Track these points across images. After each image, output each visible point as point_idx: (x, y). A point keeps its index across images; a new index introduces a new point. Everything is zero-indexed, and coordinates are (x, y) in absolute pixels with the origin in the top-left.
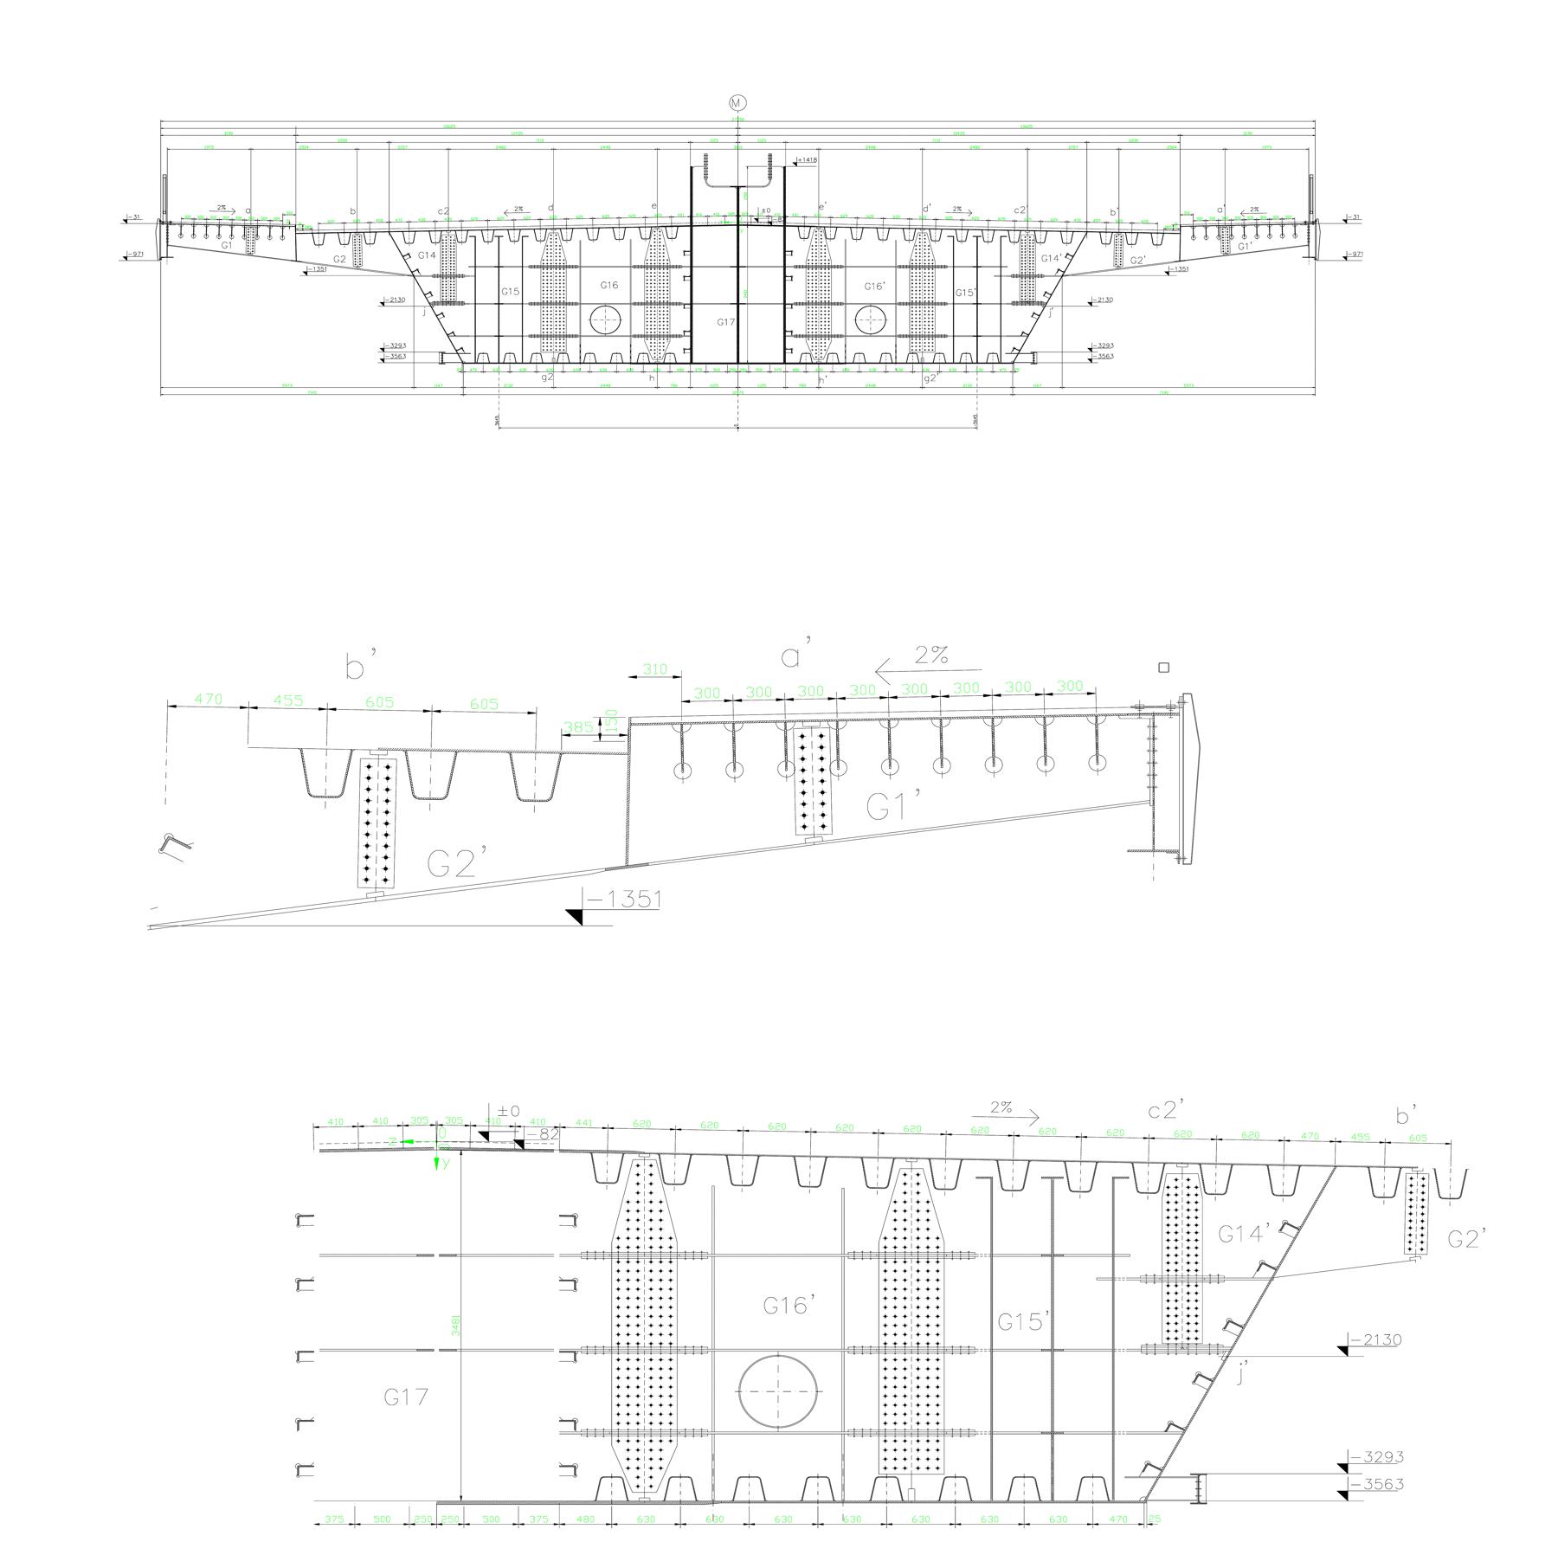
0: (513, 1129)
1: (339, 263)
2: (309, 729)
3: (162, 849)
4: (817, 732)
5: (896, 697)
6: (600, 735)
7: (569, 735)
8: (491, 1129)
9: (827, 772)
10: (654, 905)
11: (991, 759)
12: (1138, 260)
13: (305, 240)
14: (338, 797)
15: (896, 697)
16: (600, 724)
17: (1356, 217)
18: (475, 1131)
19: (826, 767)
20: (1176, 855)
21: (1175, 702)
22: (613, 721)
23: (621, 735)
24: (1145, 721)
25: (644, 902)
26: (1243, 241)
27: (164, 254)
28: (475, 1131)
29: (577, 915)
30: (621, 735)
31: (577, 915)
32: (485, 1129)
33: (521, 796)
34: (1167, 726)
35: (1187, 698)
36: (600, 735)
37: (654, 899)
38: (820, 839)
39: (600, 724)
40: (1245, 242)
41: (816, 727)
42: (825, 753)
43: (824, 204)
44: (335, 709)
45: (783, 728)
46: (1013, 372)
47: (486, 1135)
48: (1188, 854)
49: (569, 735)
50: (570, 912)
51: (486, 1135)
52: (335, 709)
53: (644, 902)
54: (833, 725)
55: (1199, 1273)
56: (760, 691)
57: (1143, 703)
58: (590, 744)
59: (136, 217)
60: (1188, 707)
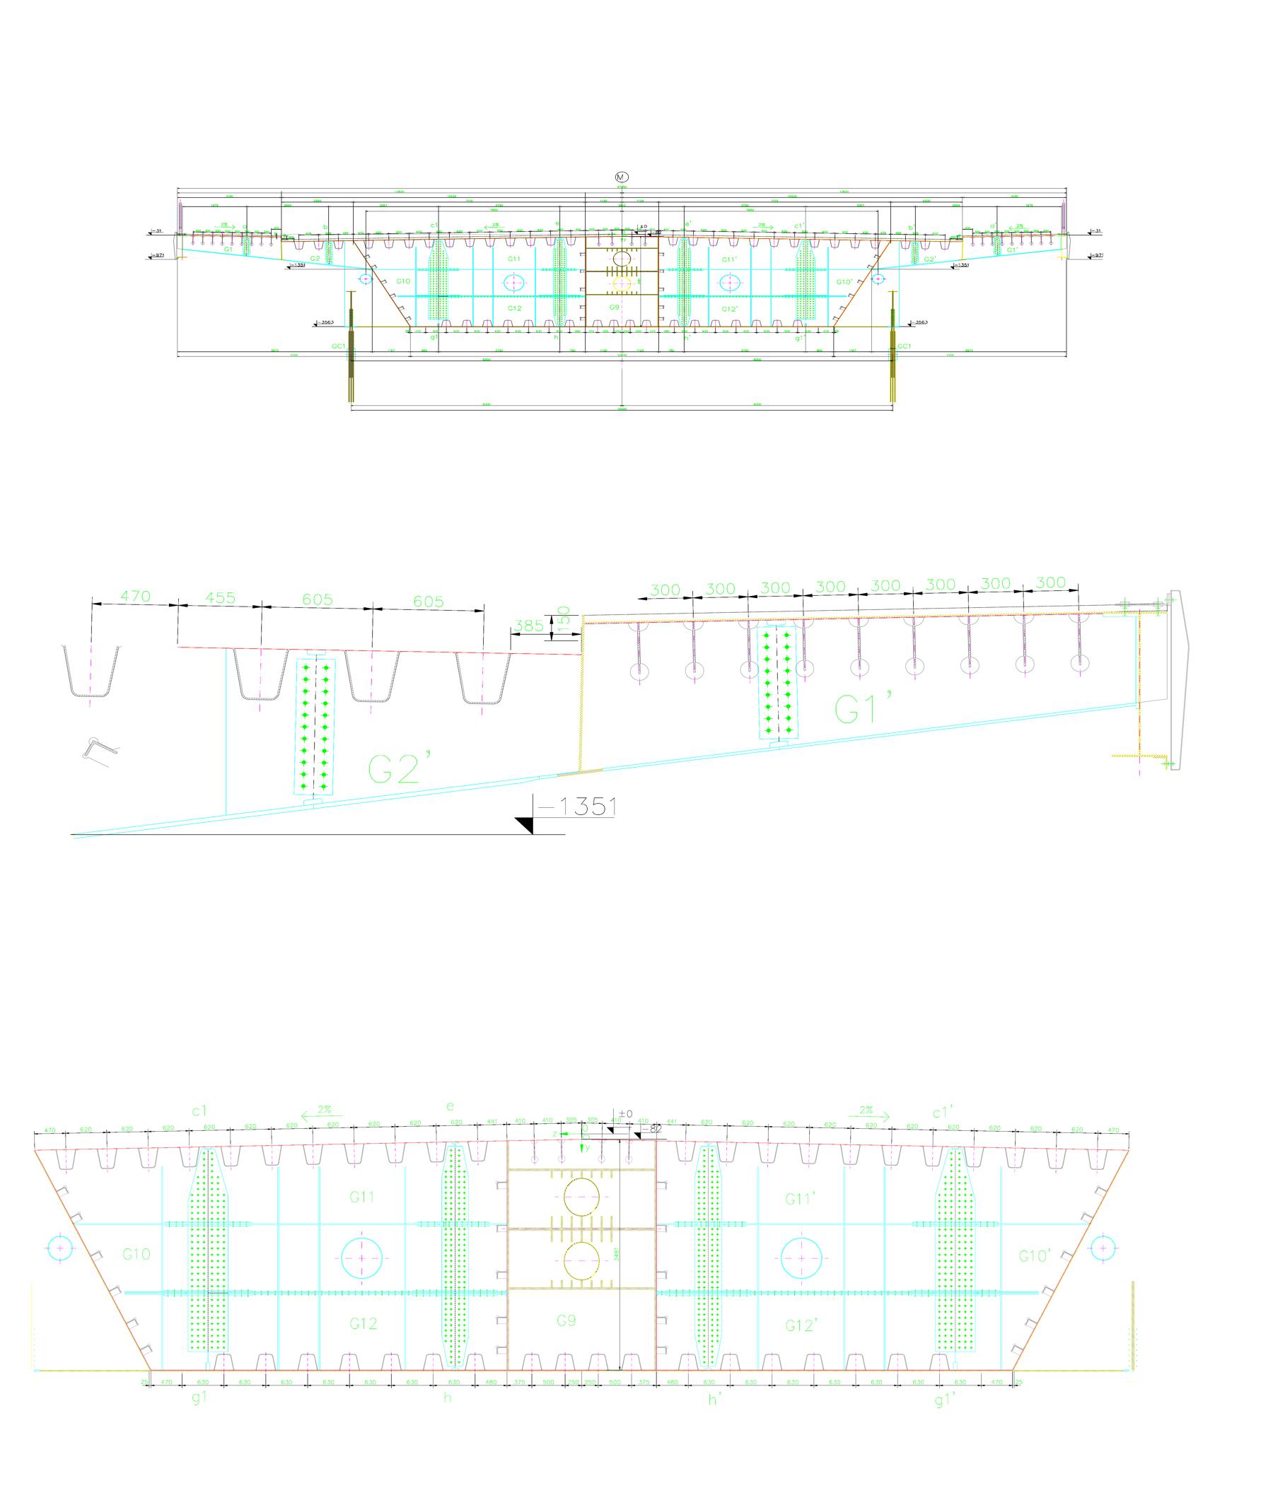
0: (628, 1126)
1: (314, 259)
2: (243, 627)
3: (86, 754)
4: (781, 631)
5: (976, 592)
6: (552, 634)
7: (518, 634)
8: (615, 1125)
9: (793, 673)
10: (609, 813)
11: (857, 662)
12: (930, 259)
13: (288, 246)
14: (354, 698)
15: (976, 592)
16: (552, 622)
17: (1098, 231)
18: (605, 1127)
19: (792, 668)
20: (1163, 760)
21: (1163, 599)
22: (565, 619)
23: (574, 634)
24: (1130, 621)
25: (599, 809)
26: (1011, 246)
27: (179, 255)
28: (605, 1127)
29: (527, 823)
30: (574, 634)
31: (527, 823)
32: (611, 1126)
33: (385, 698)
34: (1154, 625)
35: (1176, 596)
36: (552, 634)
37: (609, 806)
38: (785, 744)
39: (552, 622)
40: (1013, 247)
41: (782, 626)
42: (790, 653)
43: (689, 222)
44: (365, 609)
45: (747, 628)
46: (834, 332)
47: (611, 1129)
48: (1176, 758)
49: (518, 634)
50: (520, 820)
51: (611, 1129)
52: (270, 607)
53: (599, 809)
54: (800, 623)
55: (938, 1298)
56: (995, 582)
57: (1130, 600)
58: (540, 643)
59: (159, 231)
60: (1176, 605)
